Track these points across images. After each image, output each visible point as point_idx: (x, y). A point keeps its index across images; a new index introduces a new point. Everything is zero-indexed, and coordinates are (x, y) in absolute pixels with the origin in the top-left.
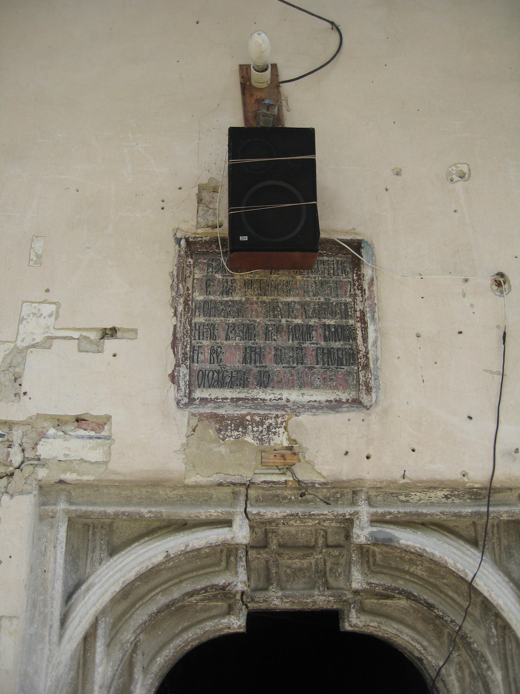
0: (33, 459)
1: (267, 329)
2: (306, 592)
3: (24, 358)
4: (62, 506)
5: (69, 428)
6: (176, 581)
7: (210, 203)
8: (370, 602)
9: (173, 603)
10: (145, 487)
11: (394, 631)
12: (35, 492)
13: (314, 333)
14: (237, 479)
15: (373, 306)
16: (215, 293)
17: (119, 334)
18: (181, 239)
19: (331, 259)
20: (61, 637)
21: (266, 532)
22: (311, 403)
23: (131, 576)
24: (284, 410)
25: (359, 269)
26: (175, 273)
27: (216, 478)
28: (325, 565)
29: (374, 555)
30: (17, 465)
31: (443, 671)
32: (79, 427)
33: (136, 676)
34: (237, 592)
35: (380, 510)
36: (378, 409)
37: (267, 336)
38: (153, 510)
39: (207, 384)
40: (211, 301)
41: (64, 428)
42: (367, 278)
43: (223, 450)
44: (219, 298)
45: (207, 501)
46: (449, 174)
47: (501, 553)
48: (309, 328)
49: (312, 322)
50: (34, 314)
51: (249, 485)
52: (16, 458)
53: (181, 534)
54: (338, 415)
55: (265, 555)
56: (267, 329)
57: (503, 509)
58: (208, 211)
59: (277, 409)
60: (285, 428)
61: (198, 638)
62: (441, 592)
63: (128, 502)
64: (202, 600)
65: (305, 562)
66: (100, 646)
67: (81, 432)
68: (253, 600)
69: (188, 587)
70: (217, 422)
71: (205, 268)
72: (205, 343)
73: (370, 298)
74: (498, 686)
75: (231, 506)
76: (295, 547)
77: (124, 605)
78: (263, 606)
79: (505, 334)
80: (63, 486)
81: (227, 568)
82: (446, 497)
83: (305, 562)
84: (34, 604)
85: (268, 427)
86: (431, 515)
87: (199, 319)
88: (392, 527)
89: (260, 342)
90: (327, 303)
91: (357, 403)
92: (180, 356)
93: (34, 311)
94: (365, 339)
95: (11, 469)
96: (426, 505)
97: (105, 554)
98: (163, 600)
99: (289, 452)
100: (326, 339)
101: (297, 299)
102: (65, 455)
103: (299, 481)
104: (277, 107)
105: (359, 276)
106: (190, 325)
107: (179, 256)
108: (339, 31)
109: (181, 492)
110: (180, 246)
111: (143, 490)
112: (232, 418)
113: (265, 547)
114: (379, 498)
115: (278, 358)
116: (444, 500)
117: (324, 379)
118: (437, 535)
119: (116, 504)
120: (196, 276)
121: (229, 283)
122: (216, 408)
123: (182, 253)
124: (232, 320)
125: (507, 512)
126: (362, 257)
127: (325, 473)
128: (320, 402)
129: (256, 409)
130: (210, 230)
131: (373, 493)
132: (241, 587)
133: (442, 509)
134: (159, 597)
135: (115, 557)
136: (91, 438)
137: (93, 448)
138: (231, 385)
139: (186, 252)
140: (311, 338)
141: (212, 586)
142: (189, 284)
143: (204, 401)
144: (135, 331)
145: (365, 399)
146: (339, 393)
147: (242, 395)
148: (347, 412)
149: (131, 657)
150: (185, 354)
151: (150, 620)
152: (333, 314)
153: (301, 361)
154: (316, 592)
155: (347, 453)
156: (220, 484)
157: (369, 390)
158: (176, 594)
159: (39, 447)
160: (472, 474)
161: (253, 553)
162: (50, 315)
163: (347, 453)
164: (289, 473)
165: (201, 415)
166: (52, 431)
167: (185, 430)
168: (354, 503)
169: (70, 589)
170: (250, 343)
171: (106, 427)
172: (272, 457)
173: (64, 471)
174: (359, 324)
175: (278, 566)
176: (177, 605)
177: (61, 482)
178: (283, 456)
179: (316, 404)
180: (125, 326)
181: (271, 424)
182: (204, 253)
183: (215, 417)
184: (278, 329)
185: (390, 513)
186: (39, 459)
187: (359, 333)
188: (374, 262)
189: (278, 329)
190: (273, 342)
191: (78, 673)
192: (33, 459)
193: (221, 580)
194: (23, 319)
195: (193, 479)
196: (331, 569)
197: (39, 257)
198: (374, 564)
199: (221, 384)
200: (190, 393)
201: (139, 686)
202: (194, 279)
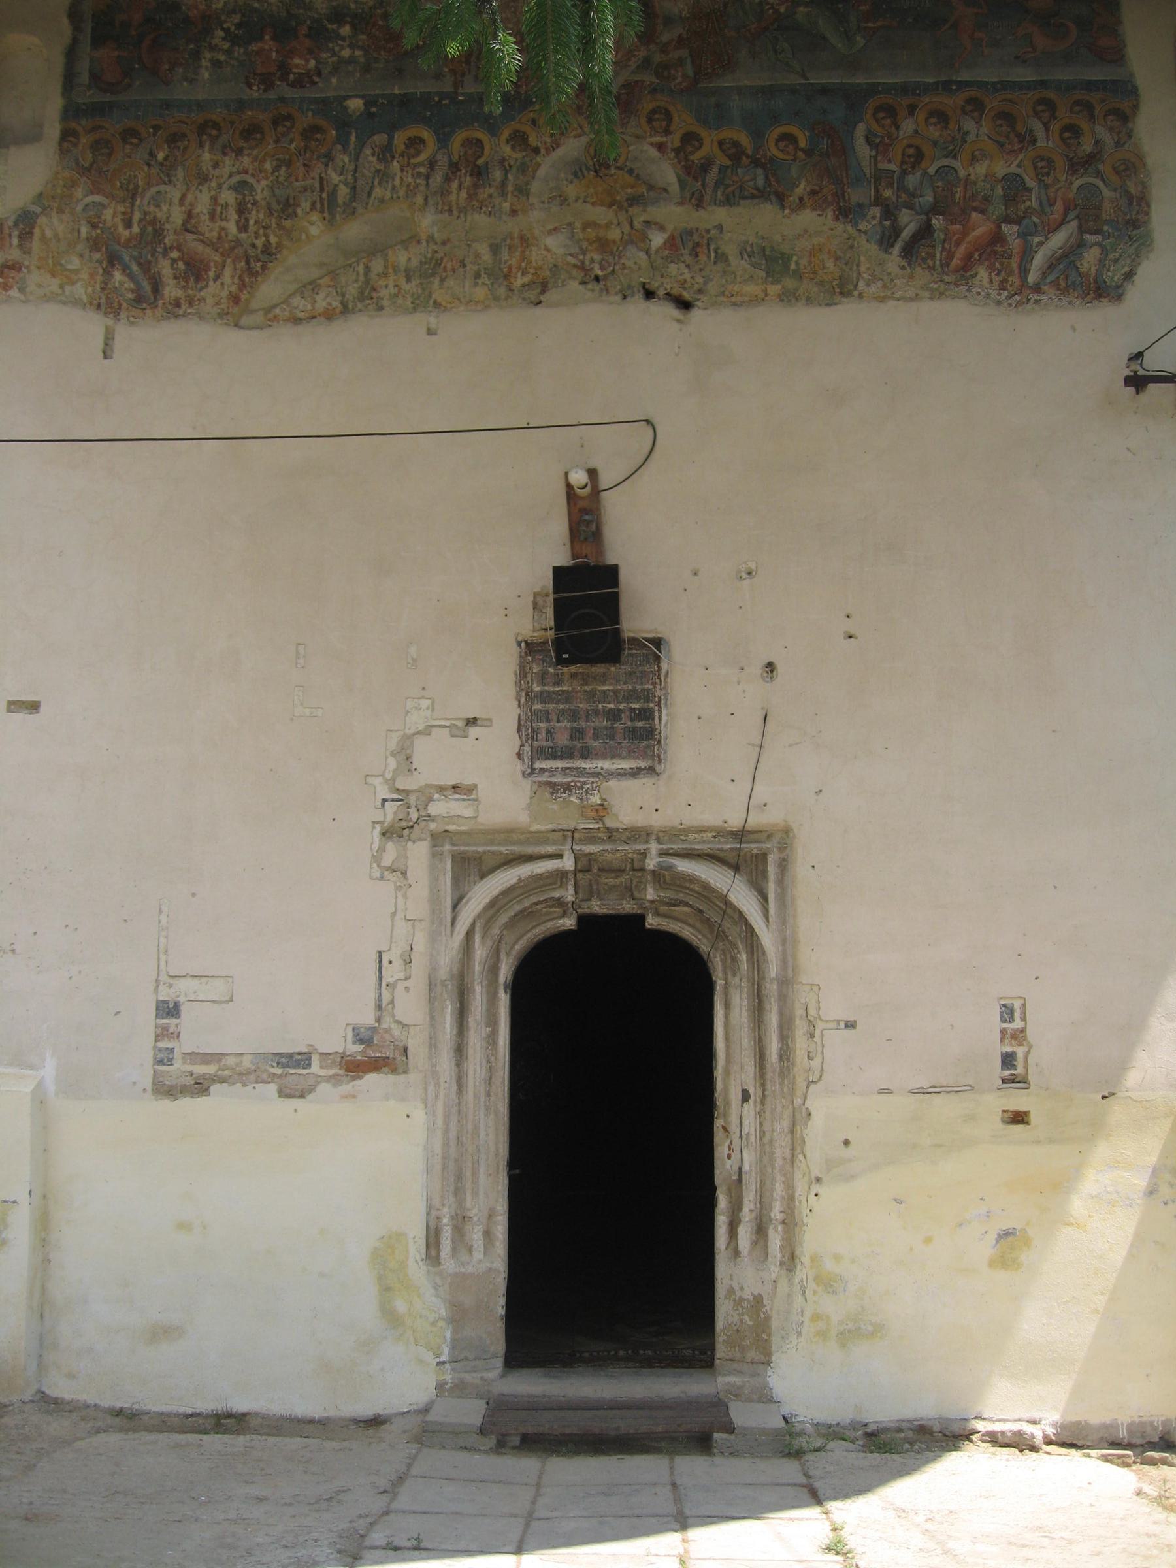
0: (425, 816)
1: (588, 712)
2: (617, 902)
3: (412, 743)
4: (447, 847)
5: (448, 793)
6: (526, 895)
7: (543, 607)
8: (663, 909)
9: (525, 909)
10: (503, 833)
11: (678, 928)
12: (429, 839)
13: (623, 715)
14: (565, 827)
15: (666, 695)
16: (548, 685)
17: (479, 722)
18: (521, 642)
19: (639, 652)
20: (452, 932)
21: (590, 860)
22: (619, 771)
23: (496, 892)
24: (598, 777)
25: (659, 662)
26: (518, 672)
27: (551, 827)
28: (631, 882)
29: (664, 876)
30: (415, 821)
31: (711, 955)
32: (455, 793)
33: (502, 958)
34: (569, 902)
35: (665, 847)
36: (664, 776)
37: (588, 719)
38: (510, 848)
39: (544, 757)
40: (546, 691)
41: (445, 793)
42: (664, 671)
43: (555, 807)
44: (552, 689)
45: (546, 841)
46: (739, 571)
47: (757, 875)
48: (619, 711)
49: (622, 706)
50: (416, 708)
51: (574, 831)
52: (414, 816)
53: (529, 864)
54: (636, 781)
55: (588, 877)
56: (588, 712)
57: (752, 846)
58: (541, 616)
59: (593, 777)
60: (599, 791)
61: (543, 933)
62: (711, 902)
63: (492, 843)
64: (545, 908)
65: (618, 881)
66: (477, 938)
67: (457, 796)
68: (580, 907)
69: (534, 899)
70: (551, 787)
71: (541, 662)
72: (542, 725)
73: (665, 688)
74: (743, 964)
75: (562, 845)
76: (611, 870)
77: (492, 912)
78: (588, 911)
79: (766, 715)
80: (448, 834)
81: (561, 886)
82: (714, 837)
83: (618, 881)
84: (433, 912)
85: (586, 791)
86: (702, 850)
87: (538, 706)
88: (674, 858)
89: (583, 723)
90: (634, 690)
91: (651, 770)
92: (524, 738)
93: (416, 705)
94: (660, 719)
95: (411, 823)
96: (699, 843)
97: (477, 878)
98: (518, 908)
99: (601, 807)
100: (632, 720)
101: (611, 688)
102: (448, 813)
103: (608, 828)
104: (594, 524)
105: (658, 667)
106: (531, 712)
107: (521, 656)
108: (655, 431)
109: (528, 835)
110: (521, 648)
111: (502, 835)
112: (561, 785)
113: (588, 871)
114: (666, 838)
115: (596, 736)
116: (713, 839)
117: (629, 751)
118: (707, 863)
119: (483, 845)
120: (534, 671)
121: (560, 676)
122: (550, 776)
123: (523, 654)
124: (561, 707)
125: (757, 848)
126: (661, 653)
127: (625, 822)
128: (625, 769)
129: (579, 777)
130: (542, 633)
131: (661, 834)
132: (570, 898)
133: (709, 846)
134: (515, 906)
135: (485, 880)
136: (464, 800)
137: (466, 807)
138: (561, 758)
139: (526, 652)
140: (620, 719)
141: (551, 898)
142: (529, 679)
143: (542, 770)
144: (490, 720)
145: (657, 767)
146: (639, 762)
147: (569, 766)
148: (644, 778)
149: (498, 945)
150: (527, 735)
151: (510, 921)
152: (638, 699)
153: (612, 737)
154: (624, 902)
155: (641, 808)
156: (554, 831)
157: (660, 761)
158: (527, 903)
159: (429, 807)
160: (730, 822)
161: (580, 875)
162: (428, 708)
163: (641, 808)
164: (601, 822)
165: (540, 782)
166: (437, 796)
167: (528, 793)
168: (647, 842)
169: (456, 902)
170: (575, 725)
171: (474, 792)
172: (589, 811)
173: (448, 824)
174: (657, 708)
175: (598, 884)
176: (260, 157)
177: (446, 831)
178: (597, 811)
179: (622, 771)
180: (484, 717)
181: (588, 788)
182: (539, 651)
183: (549, 783)
184: (596, 712)
185: (672, 849)
186: (429, 816)
187: (657, 714)
188: (670, 658)
189: (596, 712)
190: (592, 724)
191: (464, 955)
192: (425, 816)
193: (557, 894)
194: (408, 712)
195: (535, 827)
196: (636, 886)
197: (414, 660)
198: (665, 882)
199: (554, 756)
200: (532, 765)
201: (504, 964)
202: (532, 673)
